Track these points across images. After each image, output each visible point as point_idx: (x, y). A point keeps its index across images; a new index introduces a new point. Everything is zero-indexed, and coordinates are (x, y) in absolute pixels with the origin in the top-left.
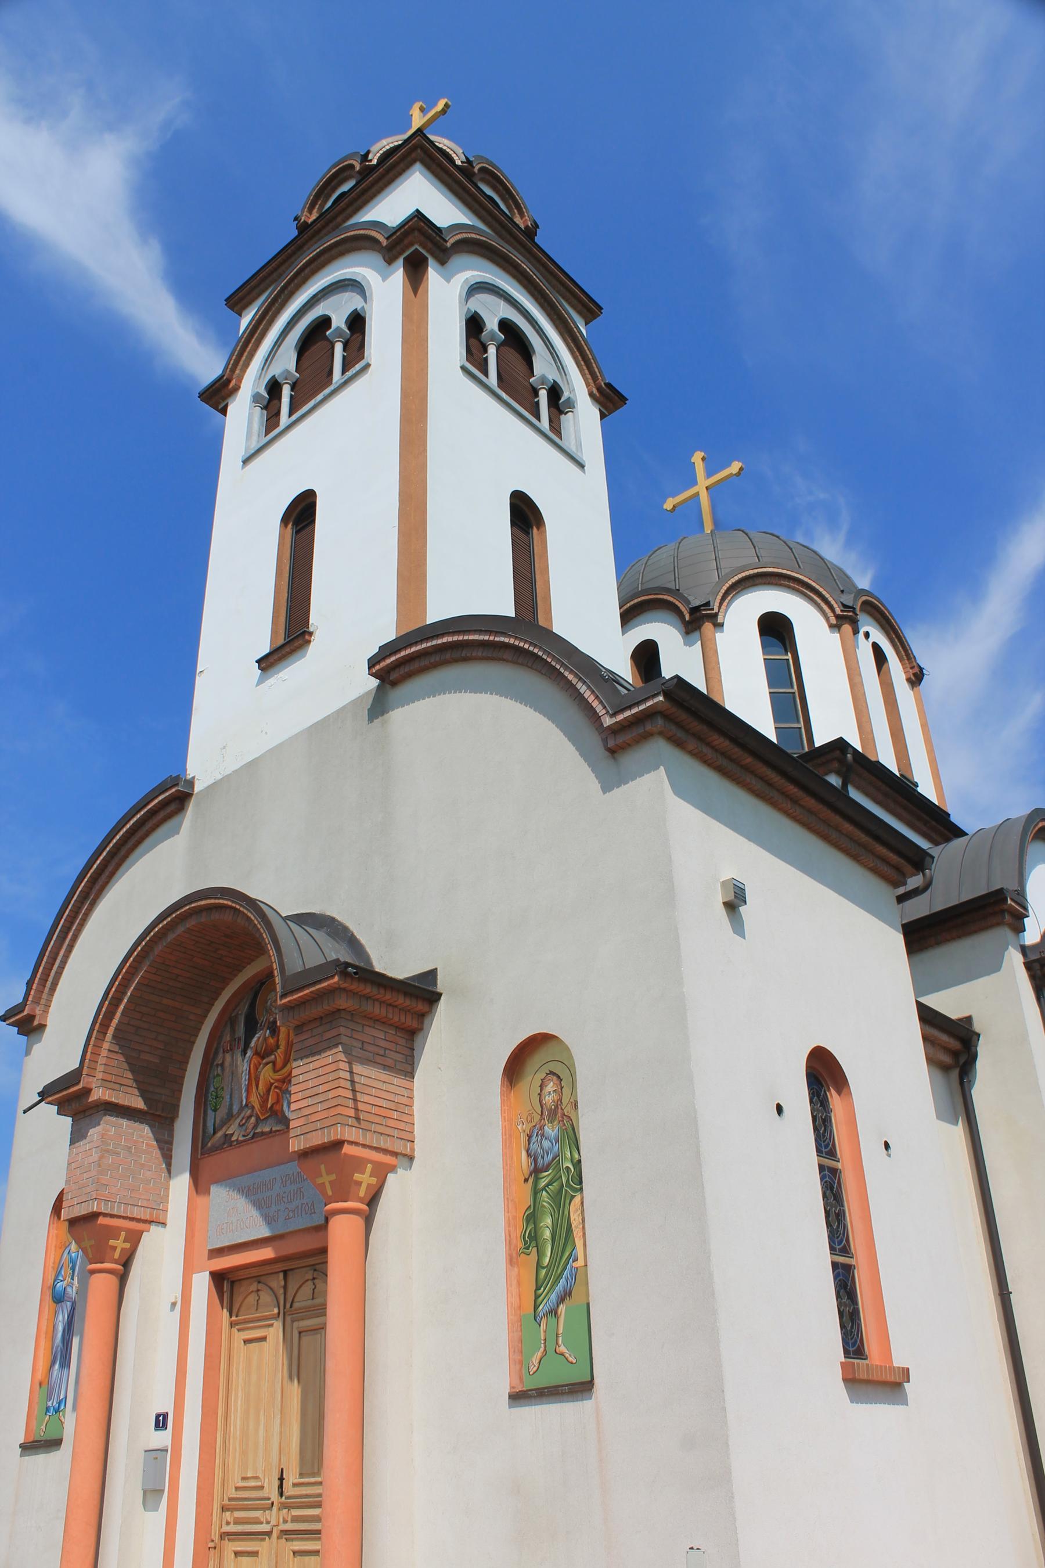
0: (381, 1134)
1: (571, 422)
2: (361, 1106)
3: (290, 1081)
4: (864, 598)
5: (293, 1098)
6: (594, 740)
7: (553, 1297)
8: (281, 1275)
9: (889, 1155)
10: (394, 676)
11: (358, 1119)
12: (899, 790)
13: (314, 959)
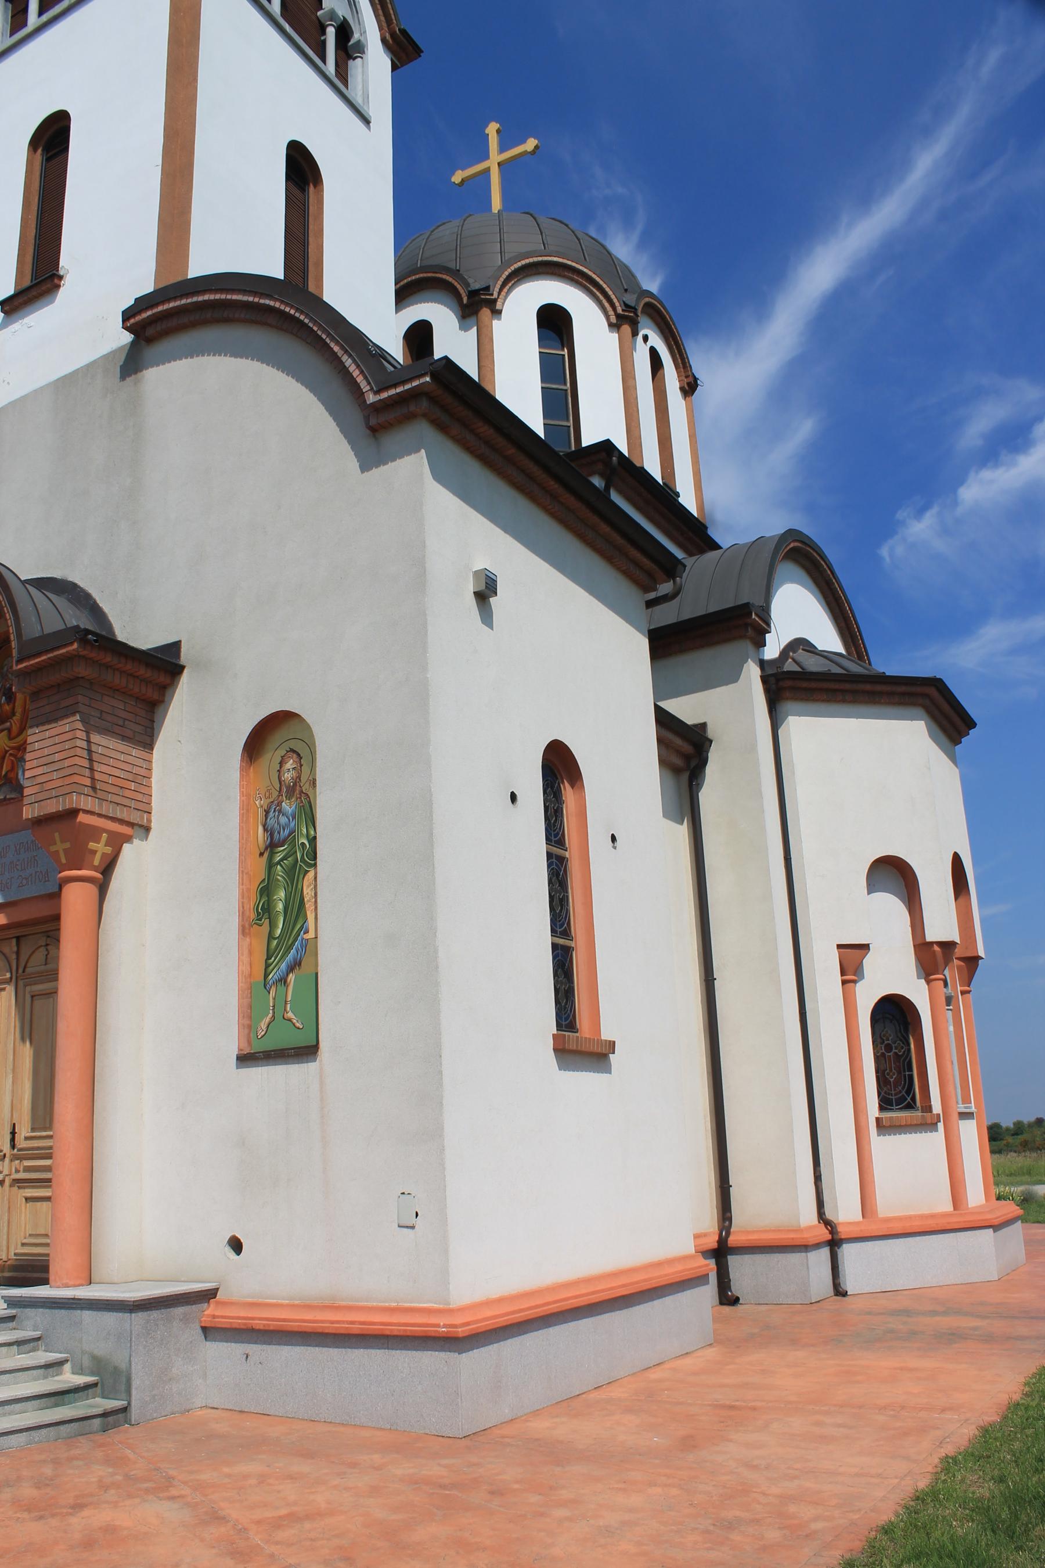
0: (118, 804)
1: (360, 70)
2: (97, 776)
3: (25, 749)
4: (647, 300)
5: (28, 765)
6: (356, 417)
7: (283, 966)
8: (14, 941)
9: (615, 848)
10: (150, 331)
11: (94, 788)
12: (660, 498)
13: (52, 624)
